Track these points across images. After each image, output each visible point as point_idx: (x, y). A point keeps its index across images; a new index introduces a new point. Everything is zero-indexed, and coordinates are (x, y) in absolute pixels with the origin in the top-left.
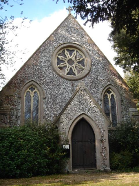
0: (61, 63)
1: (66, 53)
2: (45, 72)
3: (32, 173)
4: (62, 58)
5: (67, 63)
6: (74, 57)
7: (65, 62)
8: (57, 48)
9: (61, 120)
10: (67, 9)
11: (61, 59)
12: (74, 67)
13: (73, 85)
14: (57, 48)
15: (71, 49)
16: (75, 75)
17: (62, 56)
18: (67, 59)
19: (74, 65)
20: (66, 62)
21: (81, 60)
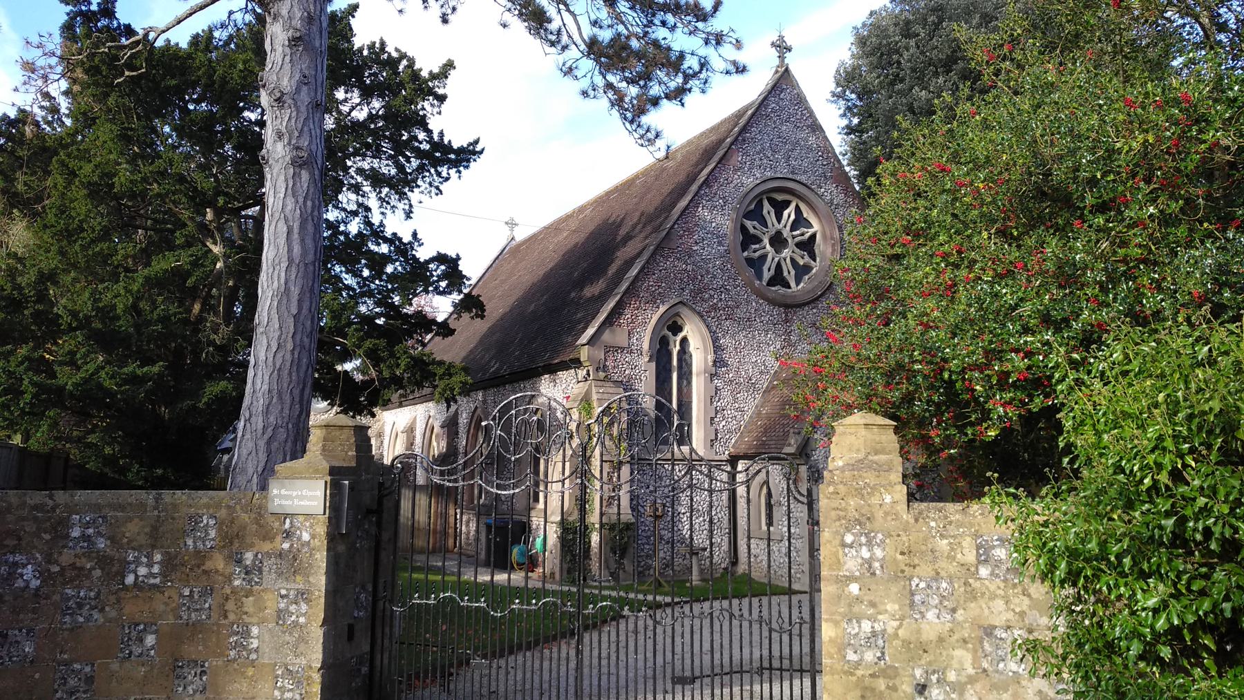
0: (754, 246)
1: (765, 212)
2: (714, 277)
3: (1214, 551)
4: (754, 228)
5: (768, 246)
6: (788, 228)
7: (762, 241)
8: (808, 303)
9: (812, 443)
10: (773, 44)
11: (752, 231)
12: (788, 260)
13: (787, 321)
14: (808, 303)
15: (780, 197)
16: (789, 287)
17: (755, 222)
18: (770, 234)
19: (786, 253)
20: (766, 241)
21: (807, 236)
